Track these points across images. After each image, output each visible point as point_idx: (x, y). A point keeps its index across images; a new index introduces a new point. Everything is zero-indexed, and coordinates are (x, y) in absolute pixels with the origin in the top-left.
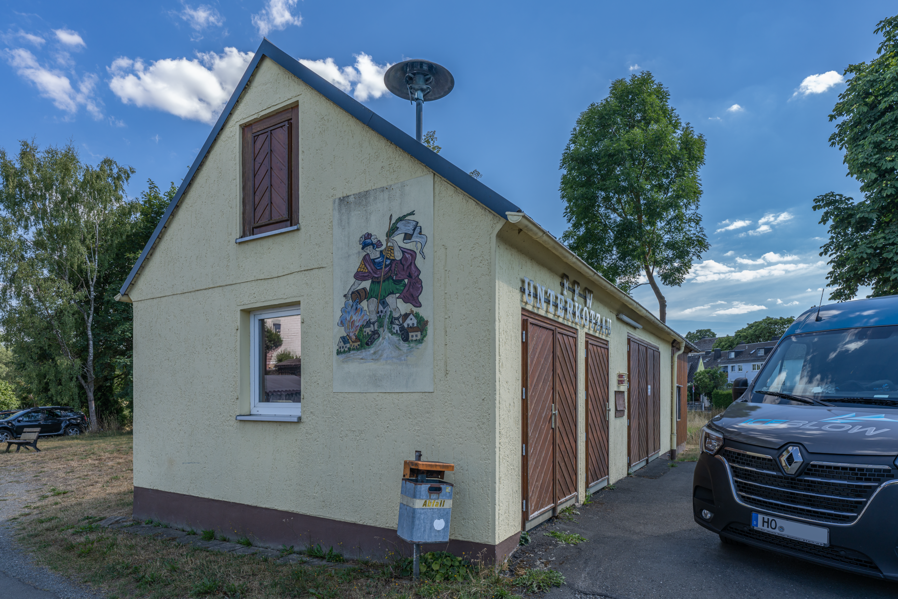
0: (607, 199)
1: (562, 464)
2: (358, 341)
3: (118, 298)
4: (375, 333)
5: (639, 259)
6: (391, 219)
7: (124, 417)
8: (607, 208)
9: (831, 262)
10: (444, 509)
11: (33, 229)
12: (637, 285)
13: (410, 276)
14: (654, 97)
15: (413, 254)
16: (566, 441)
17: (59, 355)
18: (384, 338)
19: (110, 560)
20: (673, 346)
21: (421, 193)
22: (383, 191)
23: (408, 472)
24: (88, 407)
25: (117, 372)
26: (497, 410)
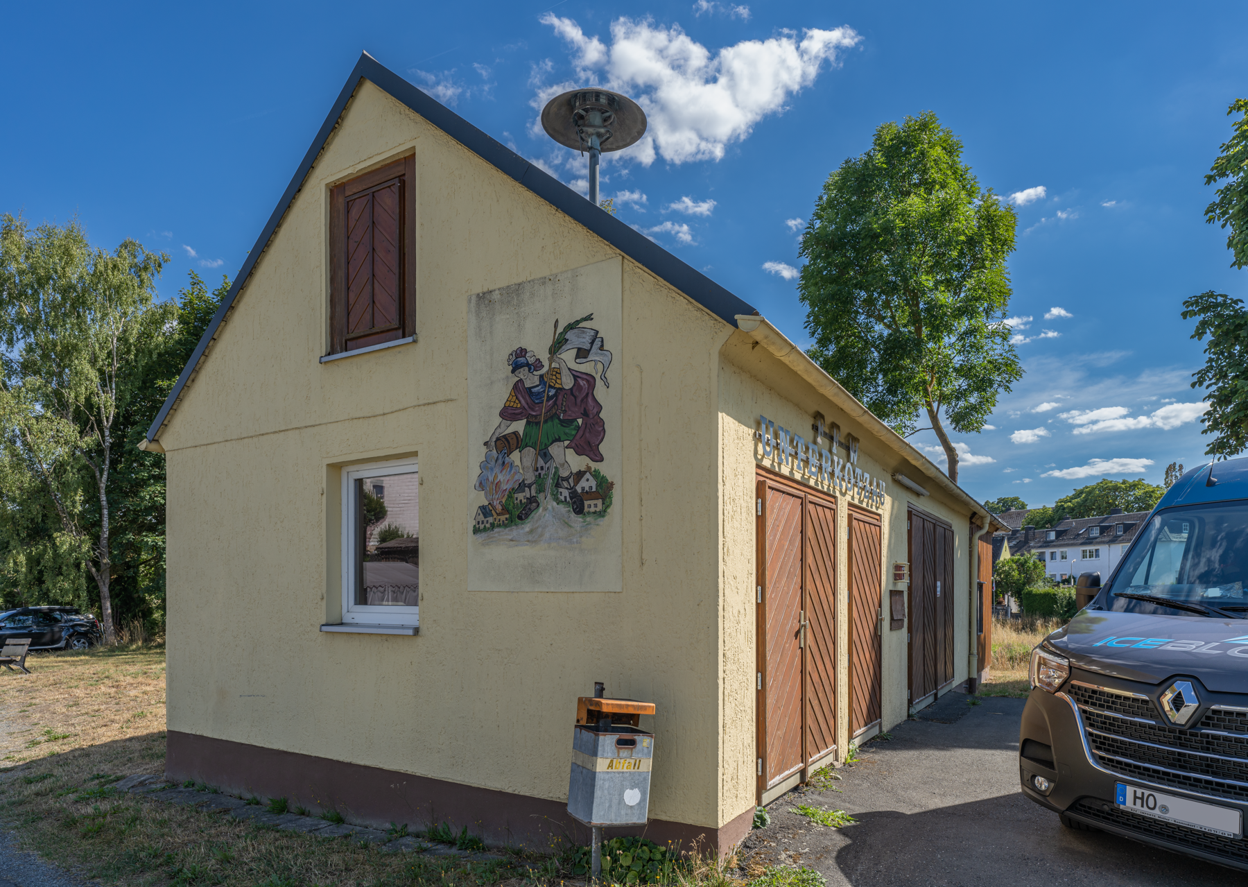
0: (870, 302)
1: (815, 703)
2: (506, 512)
3: (143, 445)
4: (532, 500)
5: (917, 390)
6: (556, 326)
7: (154, 623)
8: (869, 316)
9: (1209, 397)
10: (640, 774)
11: (20, 346)
12: (915, 431)
13: (585, 414)
14: (939, 149)
15: (591, 380)
16: (821, 667)
17: (60, 530)
18: (545, 509)
19: (130, 844)
20: (971, 523)
21: (606, 289)
22: (544, 283)
23: (584, 716)
24: (100, 608)
25: (144, 556)
26: (720, 620)
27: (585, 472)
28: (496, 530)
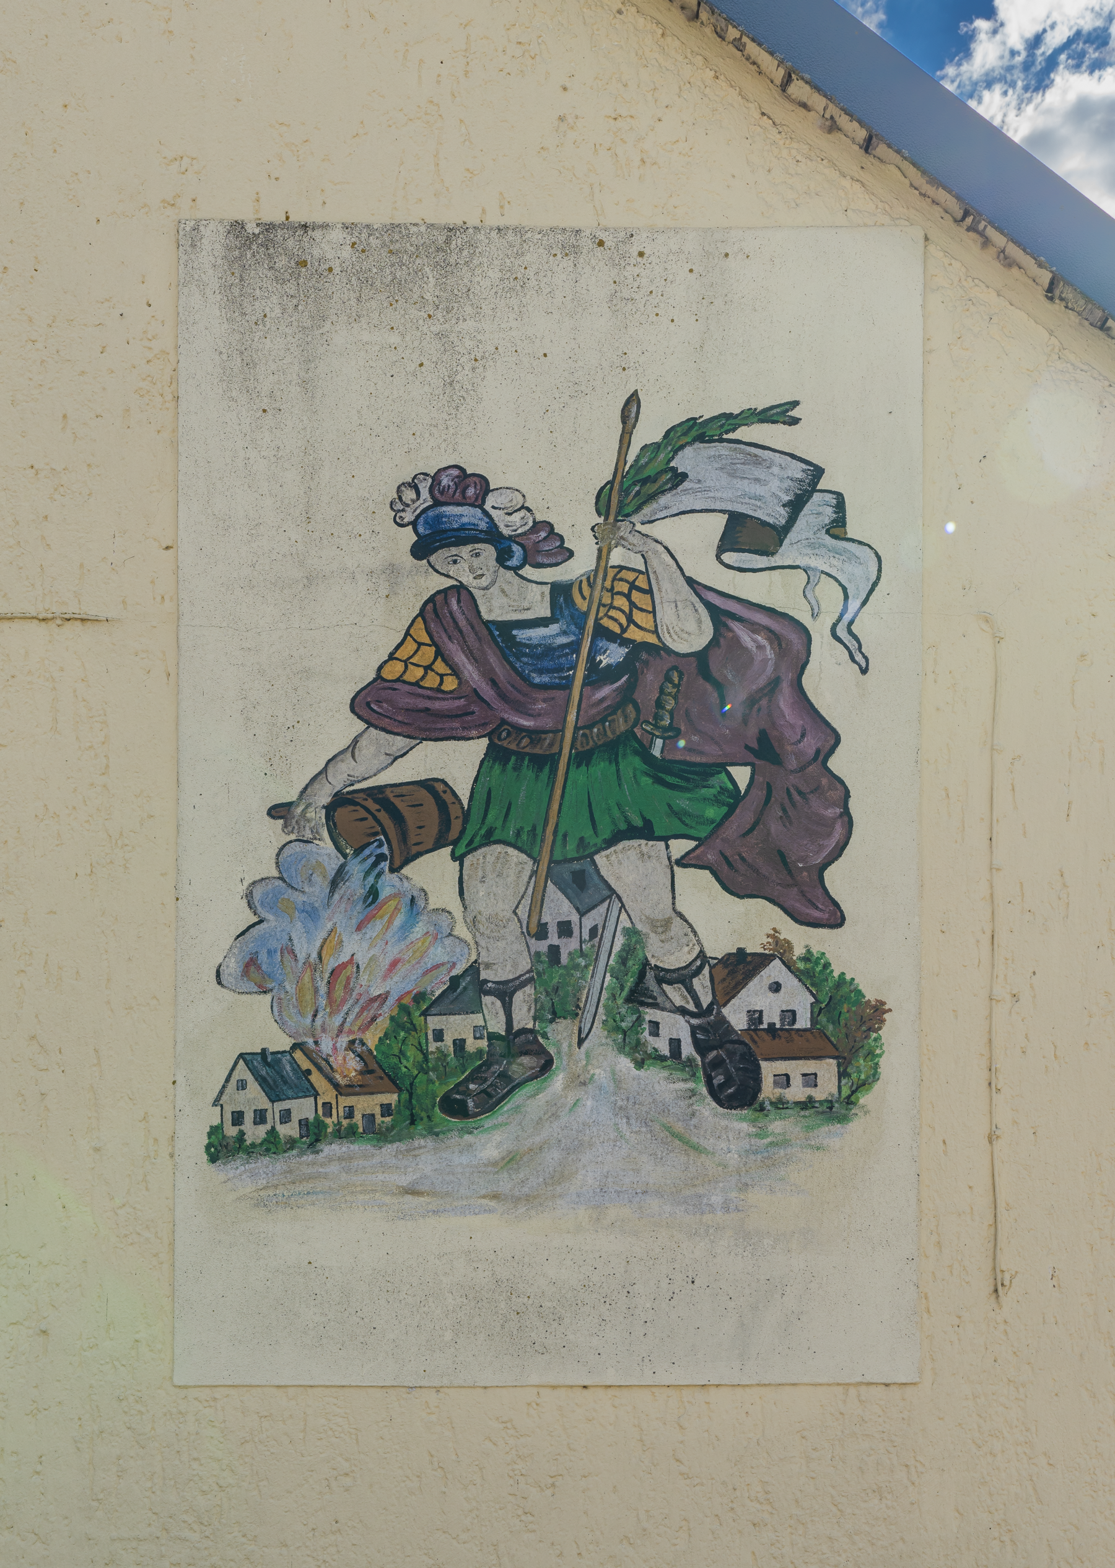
13: (765, 751)
18: (581, 1082)
22: (571, 250)
27: (761, 961)
28: (331, 1149)
